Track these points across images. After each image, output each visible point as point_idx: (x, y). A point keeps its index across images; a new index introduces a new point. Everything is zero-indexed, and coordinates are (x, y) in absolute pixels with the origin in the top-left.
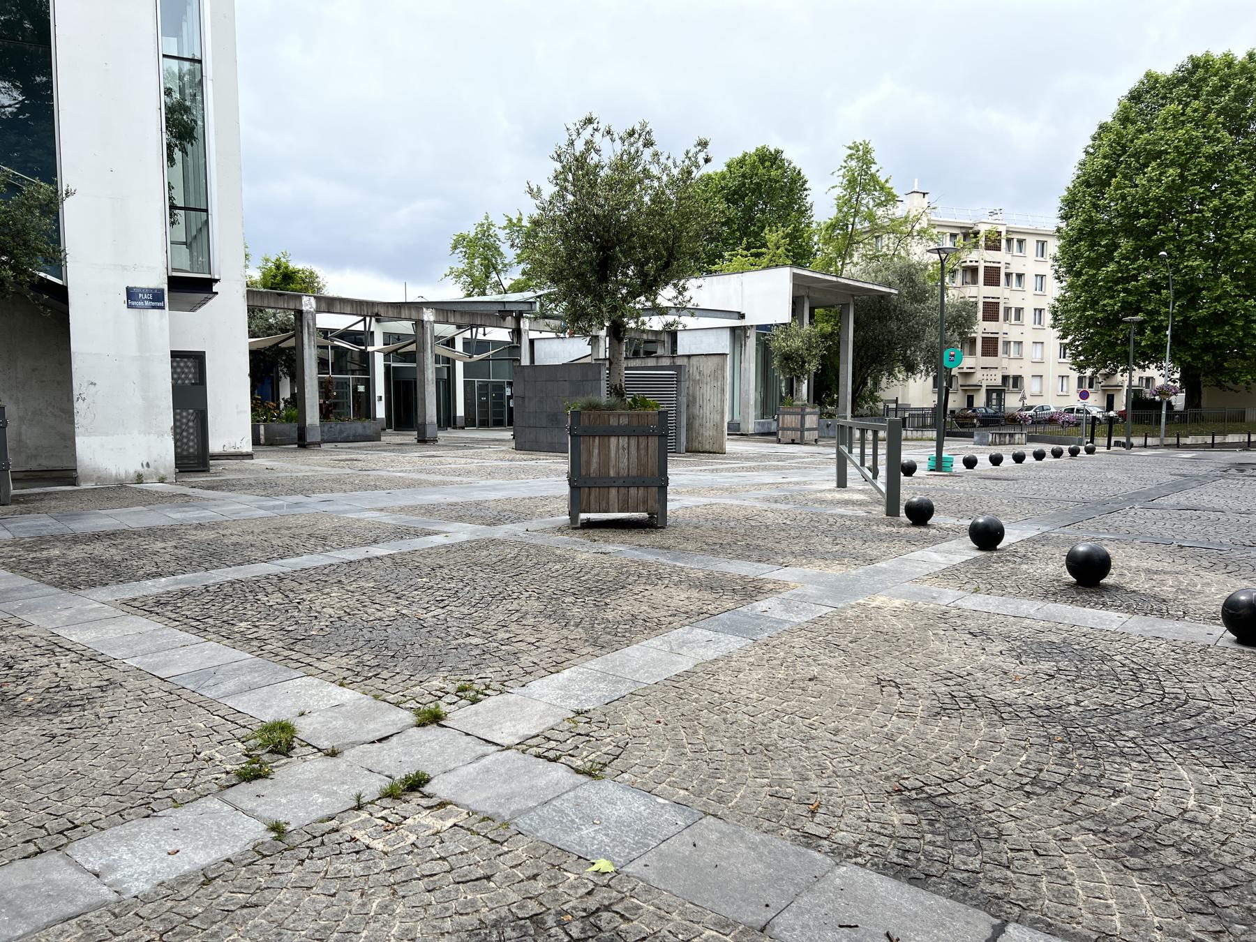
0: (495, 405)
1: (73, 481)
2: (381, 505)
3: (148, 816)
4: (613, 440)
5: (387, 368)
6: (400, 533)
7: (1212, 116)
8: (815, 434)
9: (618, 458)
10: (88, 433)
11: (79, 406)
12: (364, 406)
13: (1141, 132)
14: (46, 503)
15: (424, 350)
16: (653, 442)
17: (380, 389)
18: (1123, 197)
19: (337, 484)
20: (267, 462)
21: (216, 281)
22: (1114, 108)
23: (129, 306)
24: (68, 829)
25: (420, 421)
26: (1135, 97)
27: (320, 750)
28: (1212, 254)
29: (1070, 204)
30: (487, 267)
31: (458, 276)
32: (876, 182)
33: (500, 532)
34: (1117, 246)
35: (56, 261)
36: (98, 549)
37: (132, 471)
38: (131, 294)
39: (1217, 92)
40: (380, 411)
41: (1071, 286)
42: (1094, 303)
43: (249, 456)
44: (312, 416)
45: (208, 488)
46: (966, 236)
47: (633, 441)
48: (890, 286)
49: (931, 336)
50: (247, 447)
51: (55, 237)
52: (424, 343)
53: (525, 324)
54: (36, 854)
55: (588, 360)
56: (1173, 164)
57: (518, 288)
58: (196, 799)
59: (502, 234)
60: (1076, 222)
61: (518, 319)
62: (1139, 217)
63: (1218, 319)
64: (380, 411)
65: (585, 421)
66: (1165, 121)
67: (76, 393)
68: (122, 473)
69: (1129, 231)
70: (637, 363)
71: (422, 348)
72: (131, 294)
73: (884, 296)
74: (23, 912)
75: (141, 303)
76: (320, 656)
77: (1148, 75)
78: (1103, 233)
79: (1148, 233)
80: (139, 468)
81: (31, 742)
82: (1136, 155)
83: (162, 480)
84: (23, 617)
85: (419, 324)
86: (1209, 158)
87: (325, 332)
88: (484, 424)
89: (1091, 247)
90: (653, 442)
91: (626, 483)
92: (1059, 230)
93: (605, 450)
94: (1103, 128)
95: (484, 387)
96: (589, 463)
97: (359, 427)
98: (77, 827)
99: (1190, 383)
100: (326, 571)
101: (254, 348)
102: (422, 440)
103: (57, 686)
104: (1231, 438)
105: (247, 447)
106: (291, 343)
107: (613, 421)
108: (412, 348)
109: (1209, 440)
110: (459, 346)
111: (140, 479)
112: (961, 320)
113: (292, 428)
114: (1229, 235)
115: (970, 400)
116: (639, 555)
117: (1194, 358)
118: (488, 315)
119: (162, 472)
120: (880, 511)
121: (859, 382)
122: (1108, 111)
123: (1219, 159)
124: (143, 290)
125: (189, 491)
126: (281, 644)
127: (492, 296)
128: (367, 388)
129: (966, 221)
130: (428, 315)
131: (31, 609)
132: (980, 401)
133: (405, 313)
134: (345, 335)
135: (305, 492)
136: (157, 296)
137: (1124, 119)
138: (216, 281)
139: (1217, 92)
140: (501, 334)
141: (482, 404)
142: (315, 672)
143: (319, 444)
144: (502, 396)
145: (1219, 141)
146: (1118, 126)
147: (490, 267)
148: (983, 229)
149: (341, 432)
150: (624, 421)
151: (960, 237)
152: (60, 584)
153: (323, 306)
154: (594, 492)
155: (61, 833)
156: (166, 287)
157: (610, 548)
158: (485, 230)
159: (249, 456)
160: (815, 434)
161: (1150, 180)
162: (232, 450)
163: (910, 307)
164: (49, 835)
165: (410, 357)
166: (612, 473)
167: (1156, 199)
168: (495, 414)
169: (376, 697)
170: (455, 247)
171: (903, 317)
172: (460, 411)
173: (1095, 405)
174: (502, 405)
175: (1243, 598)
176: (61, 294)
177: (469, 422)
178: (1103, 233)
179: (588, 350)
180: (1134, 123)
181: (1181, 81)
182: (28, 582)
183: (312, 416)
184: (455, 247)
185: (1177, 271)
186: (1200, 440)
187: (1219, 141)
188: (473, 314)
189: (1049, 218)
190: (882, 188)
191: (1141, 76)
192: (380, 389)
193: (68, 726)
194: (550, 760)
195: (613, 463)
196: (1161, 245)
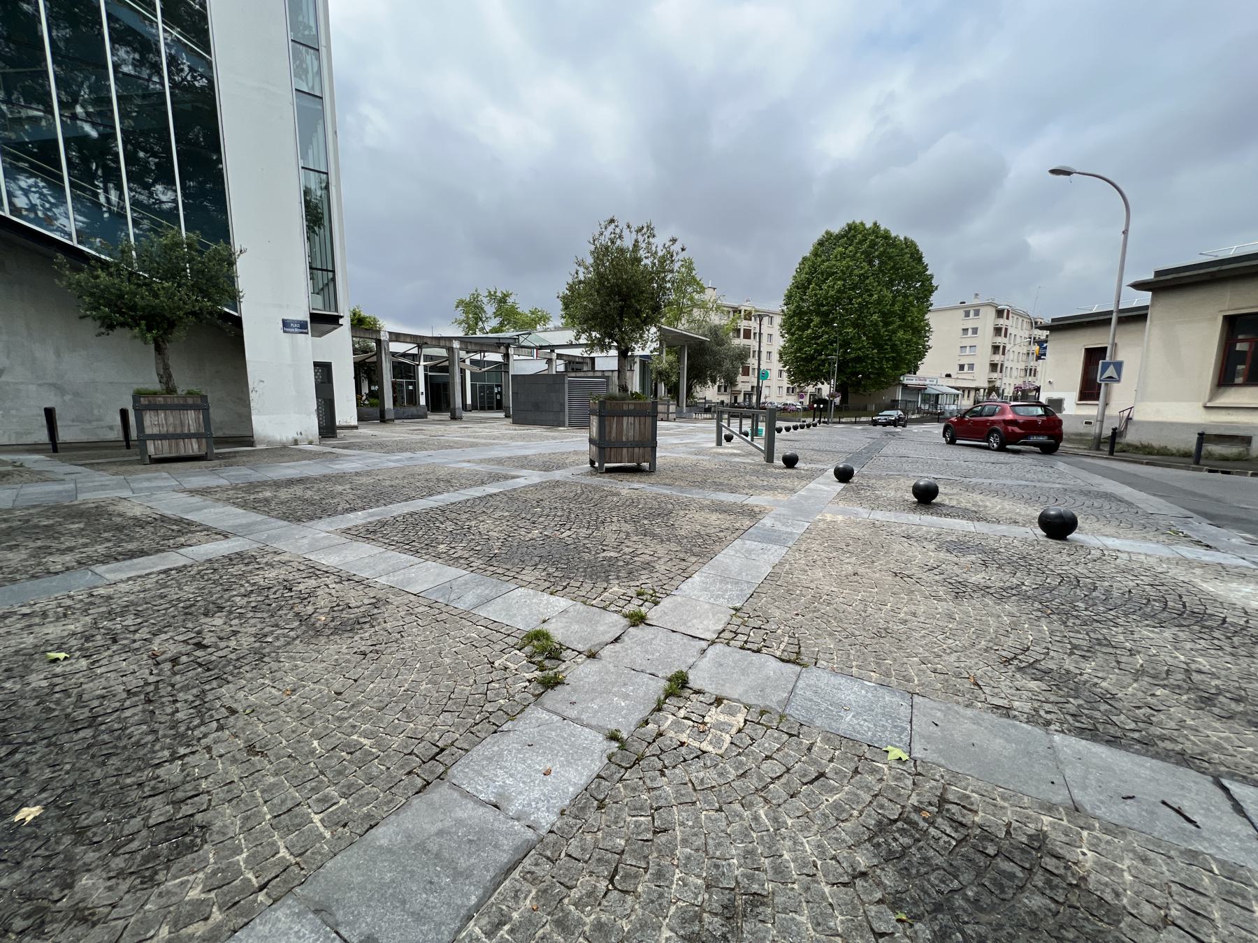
0: (488, 398)
1: (252, 444)
2: (467, 459)
3: (495, 732)
4: (625, 419)
5: (426, 376)
6: (496, 478)
7: (859, 255)
8: (674, 416)
9: (627, 430)
10: (259, 413)
11: (252, 396)
12: (413, 397)
13: (824, 261)
14: (238, 459)
15: (454, 365)
16: (649, 420)
17: (422, 388)
18: (816, 295)
19: (423, 445)
20: (367, 431)
21: (342, 317)
22: (811, 248)
23: (285, 332)
24: (437, 754)
25: (452, 406)
26: (821, 243)
27: (580, 653)
28: (855, 325)
29: (789, 298)
30: (476, 319)
31: (460, 323)
32: (695, 280)
33: (557, 475)
34: (812, 321)
35: (234, 298)
36: (298, 490)
37: (290, 438)
38: (286, 324)
39: (861, 242)
40: (422, 401)
41: (790, 340)
42: (799, 350)
43: (356, 427)
44: (389, 404)
45: (343, 448)
46: (734, 312)
47: (637, 420)
48: (705, 336)
49: (727, 365)
50: (354, 422)
51: (232, 279)
52: (453, 361)
53: (511, 351)
54: (424, 787)
55: (546, 372)
56: (840, 279)
57: (494, 330)
58: (522, 711)
59: (485, 300)
60: (792, 307)
61: (508, 347)
62: (824, 306)
63: (858, 360)
64: (422, 401)
65: (608, 407)
66: (836, 257)
67: (251, 387)
68: (284, 439)
69: (818, 313)
70: (573, 374)
71: (452, 363)
72: (286, 324)
73: (703, 342)
74: (460, 870)
75: (292, 330)
76: (518, 570)
77: (827, 233)
78: (805, 313)
79: (826, 314)
80: (295, 436)
81: (348, 661)
82: (822, 273)
83: (310, 443)
84: (275, 545)
85: (450, 350)
86: (859, 276)
87: (393, 354)
88: (482, 409)
89: (800, 320)
90: (649, 420)
91: (633, 445)
92: (783, 311)
93: (620, 424)
94: (805, 259)
95: (482, 387)
96: (610, 432)
97: (413, 410)
98: (442, 750)
99: (841, 389)
100: (468, 504)
101: (358, 360)
102: (454, 418)
103: (338, 605)
104: (863, 419)
105: (354, 422)
106: (374, 359)
107: (625, 408)
108: (446, 363)
109: (853, 420)
110: (468, 362)
111: (296, 442)
112: (743, 355)
113: (376, 411)
114: (866, 317)
115: (736, 399)
116: (656, 490)
117: (847, 378)
118: (488, 345)
119: (311, 438)
120: (761, 459)
121: (689, 389)
122: (807, 251)
123: (863, 277)
124: (294, 322)
125: (334, 450)
126: (481, 562)
127: (479, 334)
128: (415, 387)
129: (736, 305)
130: (456, 345)
131: (278, 538)
132: (740, 399)
133: (442, 343)
134: (404, 355)
135: (413, 450)
136: (303, 326)
137: (816, 254)
138: (342, 317)
139: (861, 242)
140: (496, 357)
141: (480, 397)
142: (524, 584)
143: (393, 420)
144: (492, 392)
145: (862, 268)
146: (813, 257)
147: (478, 319)
148: (743, 308)
149: (404, 413)
150: (632, 407)
151: (732, 314)
152: (285, 517)
153: (394, 338)
154: (613, 451)
155: (433, 758)
156: (309, 320)
157: (636, 486)
158: (475, 297)
159: (356, 427)
160: (674, 416)
161: (829, 287)
162: (345, 424)
163: (716, 348)
164: (424, 763)
165: (445, 369)
166: (624, 439)
167: (832, 297)
168: (488, 403)
169: (584, 603)
170: (457, 307)
171: (714, 354)
172: (469, 401)
173: (792, 400)
174: (493, 398)
175: (1052, 513)
176: (238, 322)
177: (474, 407)
178: (805, 313)
179: (546, 366)
180: (820, 256)
181: (843, 237)
182: (260, 517)
183: (389, 404)
184: (457, 307)
185: (841, 334)
186: (848, 419)
187: (862, 268)
188: (482, 344)
189: (777, 305)
190: (698, 284)
191: (823, 233)
192: (422, 388)
193: (369, 643)
194: (754, 651)
195: (625, 432)
196: (833, 320)
